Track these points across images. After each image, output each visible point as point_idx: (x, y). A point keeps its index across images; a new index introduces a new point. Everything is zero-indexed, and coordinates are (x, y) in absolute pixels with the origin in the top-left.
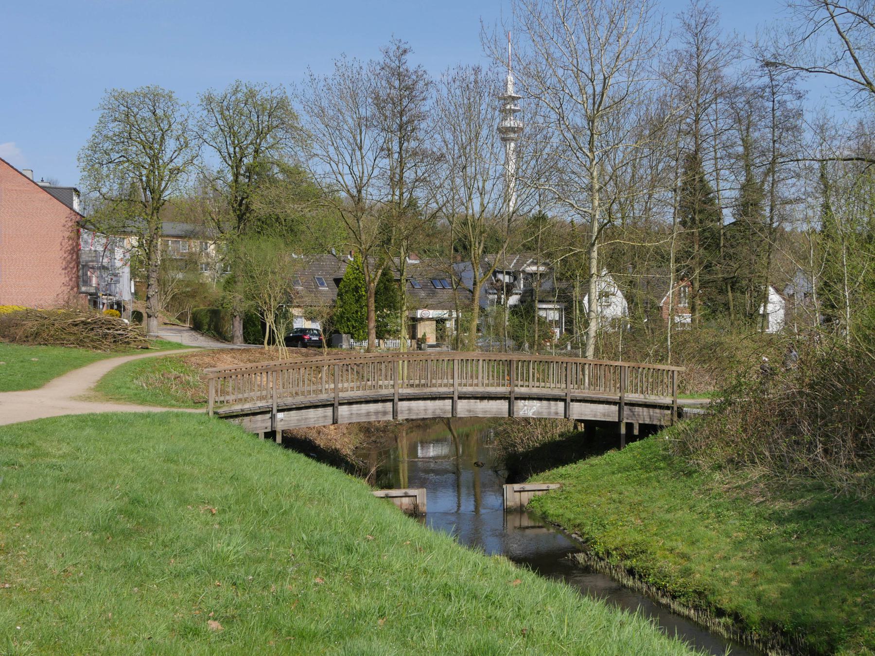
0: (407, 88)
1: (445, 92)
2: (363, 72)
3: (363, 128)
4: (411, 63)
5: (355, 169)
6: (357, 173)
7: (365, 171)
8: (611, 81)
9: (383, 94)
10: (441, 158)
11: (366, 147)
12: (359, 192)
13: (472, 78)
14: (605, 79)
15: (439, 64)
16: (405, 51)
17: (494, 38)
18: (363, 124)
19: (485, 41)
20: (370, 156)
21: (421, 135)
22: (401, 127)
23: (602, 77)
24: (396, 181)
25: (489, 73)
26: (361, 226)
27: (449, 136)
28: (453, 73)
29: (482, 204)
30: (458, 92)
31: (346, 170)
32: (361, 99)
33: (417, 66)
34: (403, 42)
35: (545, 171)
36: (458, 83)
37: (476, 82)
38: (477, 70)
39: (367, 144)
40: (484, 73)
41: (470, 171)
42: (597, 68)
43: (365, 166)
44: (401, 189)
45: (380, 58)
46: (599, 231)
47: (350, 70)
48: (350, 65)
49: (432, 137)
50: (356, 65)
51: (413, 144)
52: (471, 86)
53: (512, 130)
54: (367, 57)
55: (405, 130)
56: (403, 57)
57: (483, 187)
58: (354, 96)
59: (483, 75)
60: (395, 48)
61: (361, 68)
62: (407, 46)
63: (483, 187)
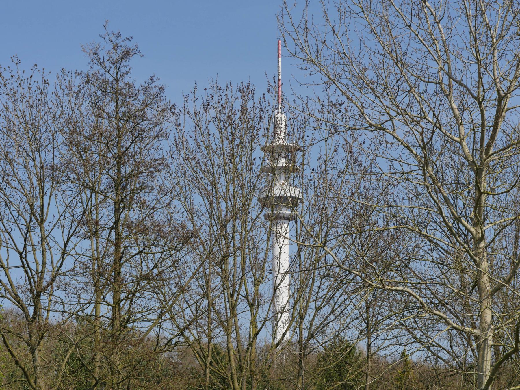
0: (130, 116)
1: (189, 125)
2: (50, 90)
3: (47, 186)
4: (137, 74)
5: (30, 257)
6: (33, 266)
7: (49, 262)
8: (509, 103)
9: (87, 124)
10: (188, 239)
11: (50, 218)
12: (36, 299)
13: (237, 105)
14: (500, 99)
15: (181, 78)
16: (127, 53)
17: (303, 26)
18: (50, 176)
19: (288, 27)
20: (58, 236)
21: (149, 197)
22: (118, 184)
23: (495, 95)
24: (105, 276)
25: (267, 96)
26: (39, 359)
27: (198, 201)
28: (203, 95)
29: (253, 323)
30: (213, 128)
31: (15, 259)
32: (44, 138)
33: (147, 79)
34: (123, 37)
35: (376, 266)
36: (212, 112)
37: (244, 111)
38: (246, 92)
39: (54, 210)
40: (258, 95)
41: (234, 264)
42: (486, 79)
43: (48, 253)
44: (116, 292)
45: (83, 64)
46: (496, 368)
47: (26, 87)
48: (27, 76)
49: (174, 203)
50: (38, 77)
51: (134, 215)
52: (236, 118)
53: (283, 200)
54: (56, 62)
55: (124, 190)
56: (124, 63)
57: (256, 291)
58: (33, 131)
59: (257, 101)
60: (110, 47)
61: (46, 82)
62: (130, 45)
63: (256, 291)
